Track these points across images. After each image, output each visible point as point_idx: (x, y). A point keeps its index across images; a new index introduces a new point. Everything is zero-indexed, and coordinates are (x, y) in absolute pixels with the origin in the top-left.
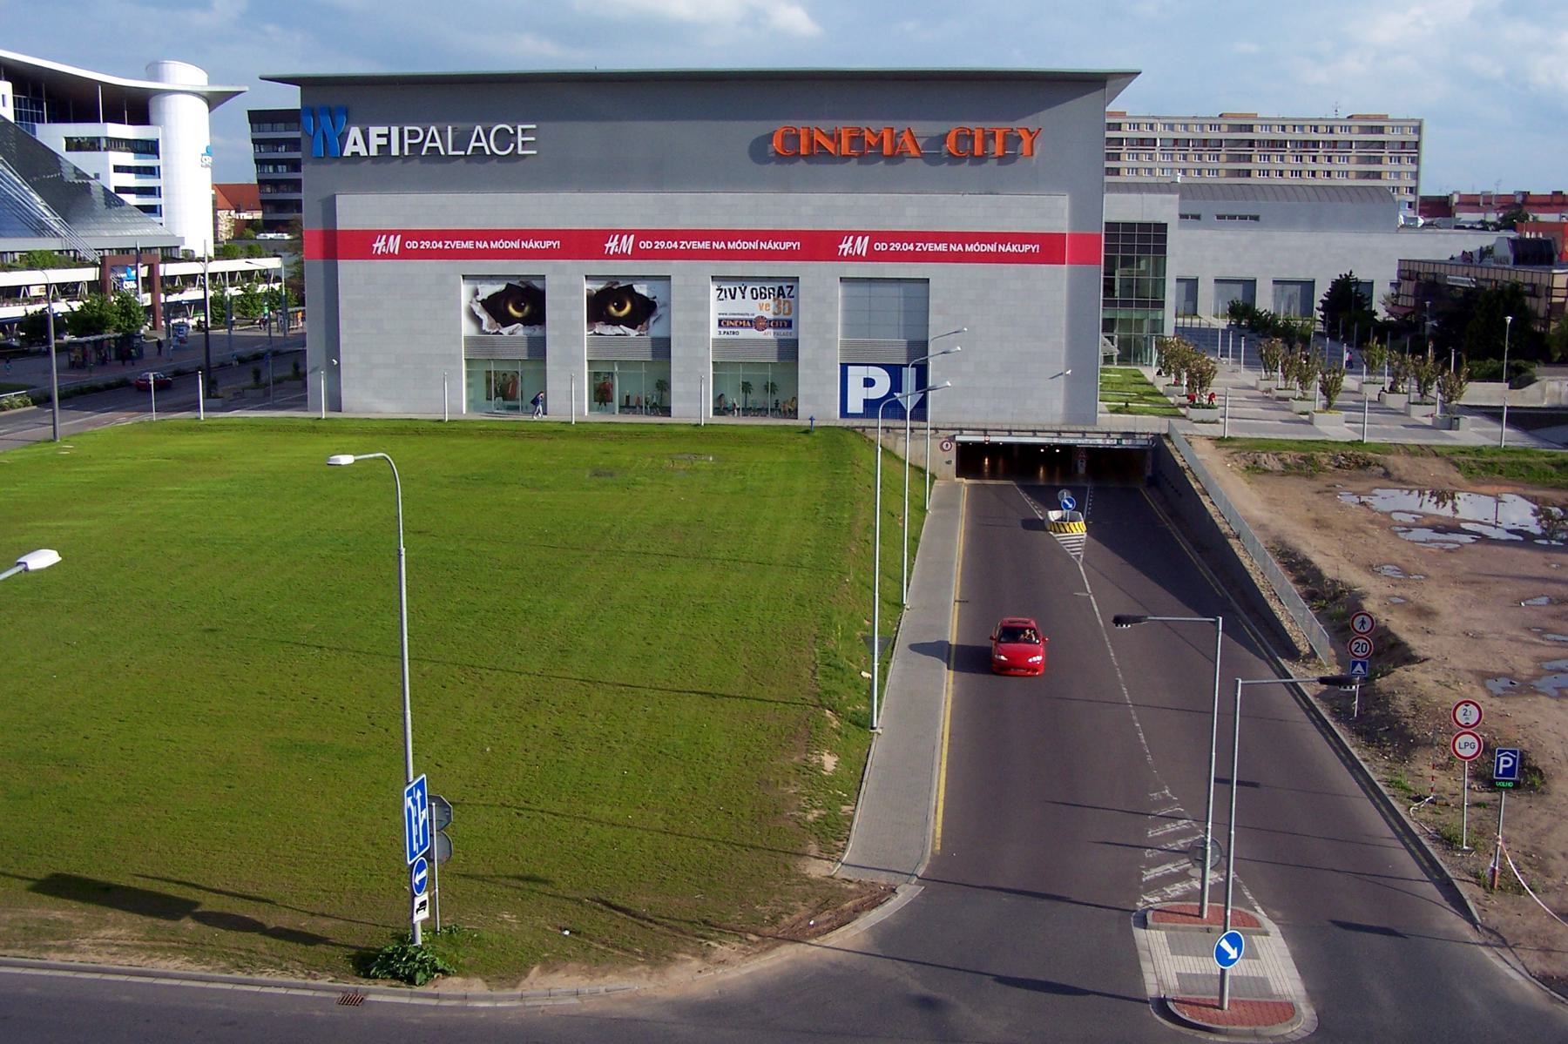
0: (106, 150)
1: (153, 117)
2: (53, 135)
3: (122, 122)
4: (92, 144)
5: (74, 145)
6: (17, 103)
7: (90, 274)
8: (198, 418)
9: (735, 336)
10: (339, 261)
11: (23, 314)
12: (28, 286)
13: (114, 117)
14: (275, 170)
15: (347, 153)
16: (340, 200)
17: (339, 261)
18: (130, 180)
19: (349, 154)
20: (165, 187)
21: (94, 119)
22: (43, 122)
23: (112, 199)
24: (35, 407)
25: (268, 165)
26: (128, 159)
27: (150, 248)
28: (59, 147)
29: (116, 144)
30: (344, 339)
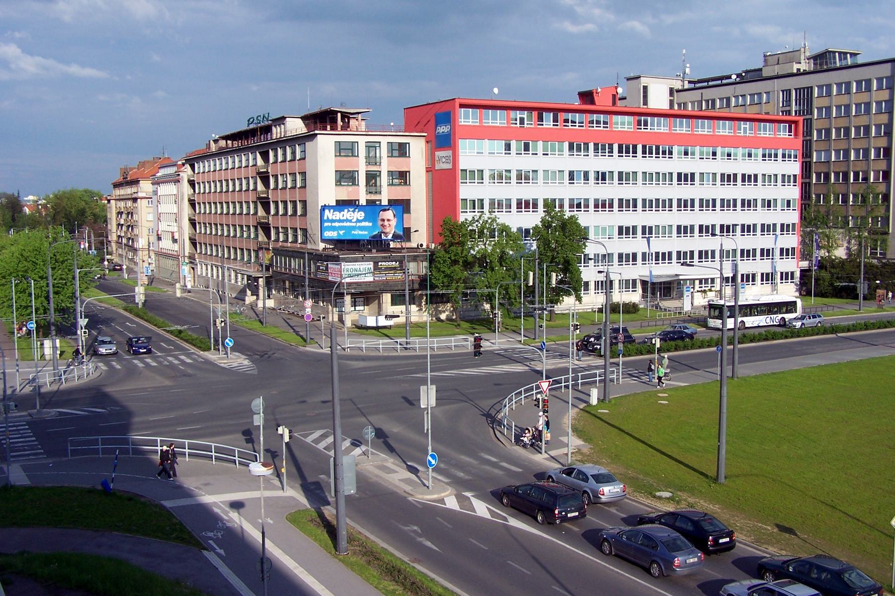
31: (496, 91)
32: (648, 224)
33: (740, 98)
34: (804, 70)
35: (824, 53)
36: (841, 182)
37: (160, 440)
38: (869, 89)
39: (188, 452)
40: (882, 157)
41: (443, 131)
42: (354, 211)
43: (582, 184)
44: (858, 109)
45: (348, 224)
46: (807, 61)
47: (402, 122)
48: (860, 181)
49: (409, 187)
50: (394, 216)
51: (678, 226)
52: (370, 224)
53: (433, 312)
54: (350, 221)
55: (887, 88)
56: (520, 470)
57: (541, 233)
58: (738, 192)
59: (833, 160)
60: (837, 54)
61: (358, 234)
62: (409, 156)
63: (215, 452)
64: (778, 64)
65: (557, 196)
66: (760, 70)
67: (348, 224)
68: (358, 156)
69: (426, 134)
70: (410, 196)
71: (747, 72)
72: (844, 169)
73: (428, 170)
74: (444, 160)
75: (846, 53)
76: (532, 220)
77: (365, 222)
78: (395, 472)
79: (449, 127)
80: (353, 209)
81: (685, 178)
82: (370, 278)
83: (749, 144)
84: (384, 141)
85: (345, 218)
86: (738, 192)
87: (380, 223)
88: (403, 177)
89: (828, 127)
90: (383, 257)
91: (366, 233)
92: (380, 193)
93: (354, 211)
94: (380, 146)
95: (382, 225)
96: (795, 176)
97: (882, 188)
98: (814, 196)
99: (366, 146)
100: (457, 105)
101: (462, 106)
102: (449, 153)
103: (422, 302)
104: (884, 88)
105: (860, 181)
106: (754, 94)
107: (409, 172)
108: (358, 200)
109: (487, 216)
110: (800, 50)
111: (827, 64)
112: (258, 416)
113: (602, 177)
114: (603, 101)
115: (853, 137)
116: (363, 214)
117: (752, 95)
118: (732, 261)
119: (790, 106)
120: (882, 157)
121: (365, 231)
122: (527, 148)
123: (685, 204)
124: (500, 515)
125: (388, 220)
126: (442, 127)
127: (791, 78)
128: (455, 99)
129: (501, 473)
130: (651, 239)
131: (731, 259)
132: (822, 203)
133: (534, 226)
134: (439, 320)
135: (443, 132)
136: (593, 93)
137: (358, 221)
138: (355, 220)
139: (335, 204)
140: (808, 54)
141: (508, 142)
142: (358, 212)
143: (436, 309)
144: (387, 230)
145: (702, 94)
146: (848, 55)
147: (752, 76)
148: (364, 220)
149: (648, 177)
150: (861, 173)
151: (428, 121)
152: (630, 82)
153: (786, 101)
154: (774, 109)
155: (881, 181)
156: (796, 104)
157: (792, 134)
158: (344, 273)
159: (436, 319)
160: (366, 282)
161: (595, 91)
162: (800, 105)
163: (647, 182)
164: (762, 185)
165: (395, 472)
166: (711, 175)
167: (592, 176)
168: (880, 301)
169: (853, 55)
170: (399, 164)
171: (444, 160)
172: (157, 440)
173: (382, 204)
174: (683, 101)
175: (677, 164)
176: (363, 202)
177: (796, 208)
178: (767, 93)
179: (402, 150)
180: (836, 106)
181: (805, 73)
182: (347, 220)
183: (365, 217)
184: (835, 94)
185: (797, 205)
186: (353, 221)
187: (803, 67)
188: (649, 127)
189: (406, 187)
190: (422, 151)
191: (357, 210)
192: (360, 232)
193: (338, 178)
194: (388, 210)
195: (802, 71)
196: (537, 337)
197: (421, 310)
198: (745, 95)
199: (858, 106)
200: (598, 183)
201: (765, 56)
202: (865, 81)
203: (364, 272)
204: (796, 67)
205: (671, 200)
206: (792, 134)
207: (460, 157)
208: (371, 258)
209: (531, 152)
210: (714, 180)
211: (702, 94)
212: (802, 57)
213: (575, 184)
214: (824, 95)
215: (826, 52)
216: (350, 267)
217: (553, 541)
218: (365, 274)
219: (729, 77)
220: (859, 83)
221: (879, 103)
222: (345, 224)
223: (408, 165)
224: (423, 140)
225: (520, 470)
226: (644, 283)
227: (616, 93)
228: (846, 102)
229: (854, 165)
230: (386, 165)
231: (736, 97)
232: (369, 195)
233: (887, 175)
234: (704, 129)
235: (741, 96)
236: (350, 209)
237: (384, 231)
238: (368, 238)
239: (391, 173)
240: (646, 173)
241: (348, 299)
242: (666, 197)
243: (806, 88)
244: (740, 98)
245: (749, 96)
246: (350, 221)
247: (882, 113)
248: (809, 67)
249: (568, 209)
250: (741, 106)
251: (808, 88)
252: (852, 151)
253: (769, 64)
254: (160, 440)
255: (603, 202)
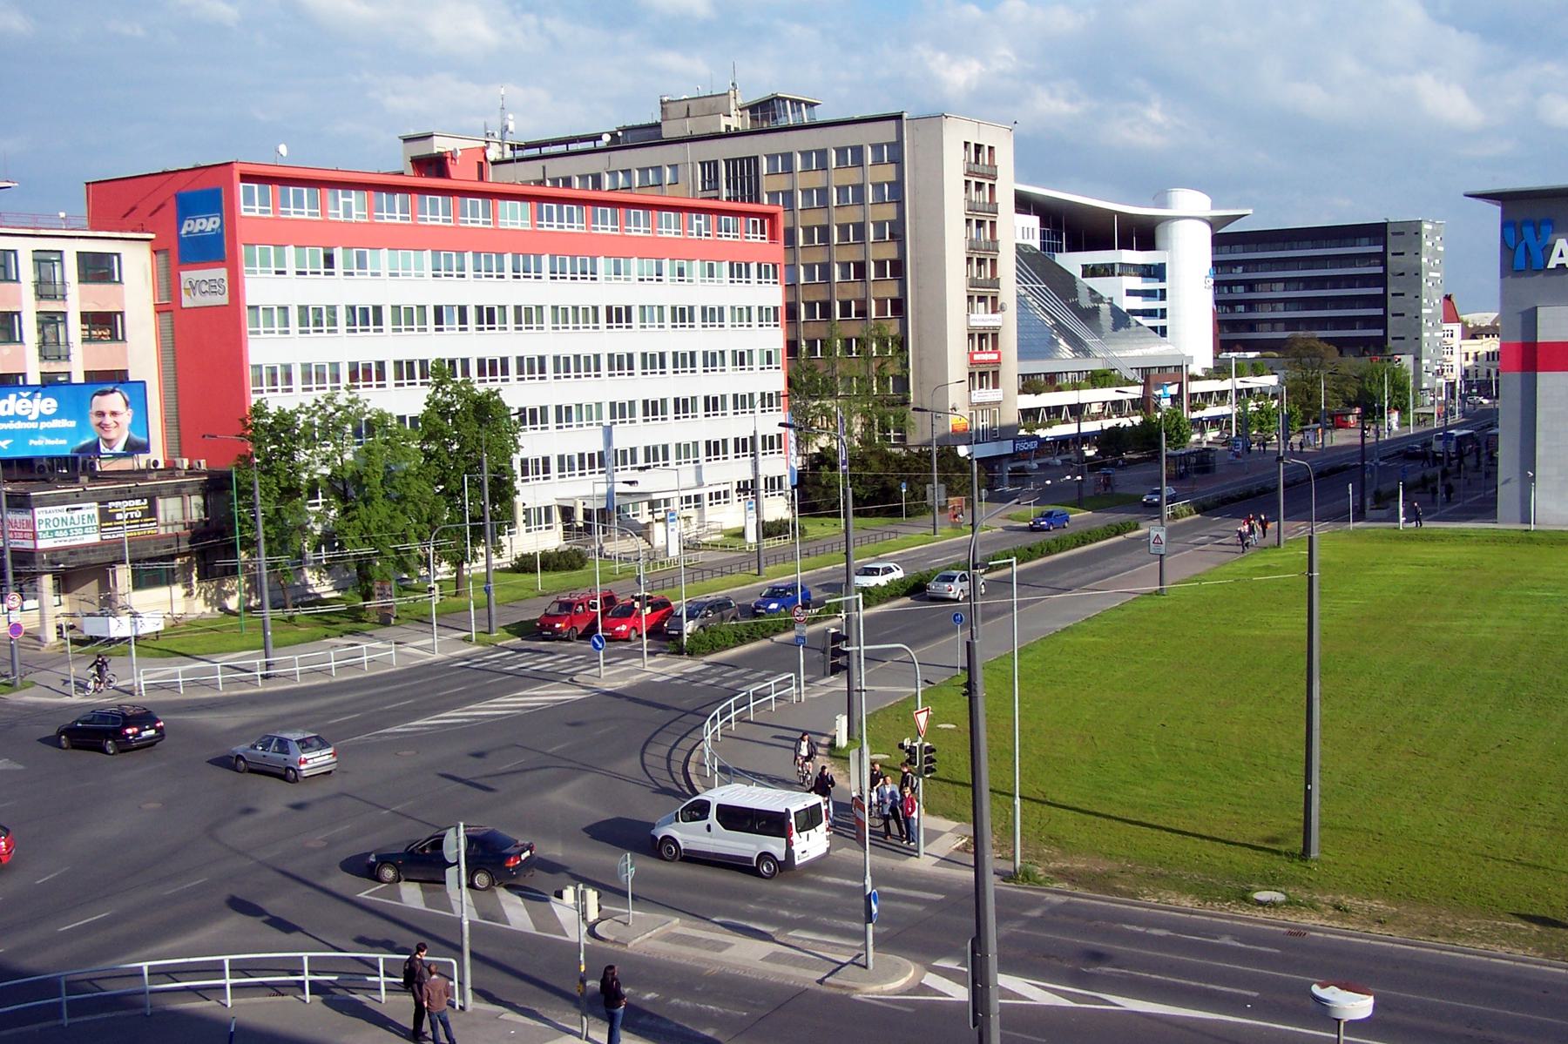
0: (1120, 275)
1: (1159, 242)
2: (1072, 262)
3: (1132, 249)
4: (1107, 270)
5: (1091, 271)
6: (1043, 235)
7: (1136, 392)
8: (1398, 528)
9: (38, 652)
10: (1538, 373)
11: (1100, 429)
12: (1090, 404)
13: (1126, 244)
14: (1230, 291)
15: (1551, 265)
16: (1541, 312)
17: (1538, 373)
18: (1138, 303)
19: (1554, 266)
20: (1170, 308)
21: (1108, 246)
22: (1061, 251)
23: (1121, 319)
24: (1198, 516)
25: (1224, 285)
26: (1137, 283)
27: (1166, 367)
28: (1077, 272)
29: (1127, 269)
30: (1540, 451)
31: (283, 149)
32: (565, 403)
33: (621, 175)
34: (736, 129)
35: (769, 101)
36: (818, 318)
37: (310, 958)
38: (823, 166)
39: (224, 978)
40: (888, 277)
41: (202, 228)
42: (31, 398)
43: (457, 331)
44: (841, 196)
45: (19, 425)
46: (740, 113)
47: (82, 210)
48: (853, 317)
49: (123, 344)
50: (127, 404)
51: (557, 407)
52: (73, 424)
53: (213, 596)
54: (24, 419)
55: (891, 162)
56: (942, 897)
57: (431, 425)
58: (697, 339)
59: (802, 281)
60: (788, 102)
61: (43, 446)
62: (120, 281)
63: (312, 972)
64: (688, 116)
65: (457, 354)
66: (658, 126)
67: (19, 425)
68: (17, 280)
69: (152, 236)
70: (126, 363)
71: (625, 130)
72: (824, 297)
73: (160, 309)
74: (205, 288)
75: (802, 102)
76: (410, 401)
77: (60, 419)
78: (728, 945)
79: (218, 220)
80: (28, 393)
81: (619, 316)
82: (94, 538)
83: (654, 251)
84: (71, 249)
85: (10, 412)
86: (697, 339)
87: (95, 420)
88: (103, 324)
89: (825, 223)
90: (117, 491)
91: (64, 442)
92: (68, 358)
93: (31, 398)
94: (61, 261)
95: (99, 425)
96: (776, 309)
97: (893, 328)
98: (804, 343)
99: (34, 260)
100: (237, 177)
101: (245, 178)
102: (221, 273)
103: (191, 578)
104: (886, 161)
105: (853, 317)
106: (647, 169)
107: (122, 313)
108: (24, 375)
109: (342, 398)
110: (727, 94)
111: (774, 118)
112: (455, 869)
113: (487, 316)
114: (462, 174)
115: (836, 242)
116: (54, 403)
117: (644, 171)
118: (694, 462)
119: (717, 189)
120: (888, 277)
121: (61, 438)
122: (361, 263)
123: (621, 363)
124: (1087, 996)
125: (114, 414)
126: (198, 221)
127: (716, 142)
128: (232, 163)
129: (920, 908)
130: (614, 426)
131: (691, 459)
132: (819, 356)
133: (387, 411)
134: (224, 609)
135: (201, 231)
136: (446, 158)
137: (43, 417)
138: (35, 416)
139: (83, 381)
140: (740, 101)
141: (328, 252)
142: (42, 398)
143: (218, 588)
144: (112, 435)
145: (544, 168)
146: (803, 105)
147: (646, 136)
148: (58, 415)
149: (563, 315)
150: (853, 303)
151: (133, 209)
152: (410, 144)
153: (710, 182)
154: (689, 189)
155: (889, 315)
156: (728, 187)
157: (766, 236)
158: (40, 528)
159: (220, 610)
160: (87, 546)
161: (449, 155)
162: (735, 188)
163: (403, 327)
164: (553, 328)
165: (728, 945)
166: (656, 309)
167: (471, 315)
168: (955, 516)
169: (810, 105)
170: (100, 298)
171: (205, 288)
172: (301, 958)
173: (74, 381)
174: (564, 175)
175: (604, 292)
176: (34, 379)
177: (780, 365)
178: (674, 167)
179: (97, 269)
180: (803, 191)
181: (739, 134)
182: (16, 417)
183: (59, 408)
184: (799, 169)
185: (781, 358)
186: (30, 418)
187: (735, 122)
188: (555, 223)
189: (114, 345)
190: (146, 271)
191: (39, 395)
192: (49, 442)
193: (40, 326)
194: (113, 391)
195: (732, 129)
196: (494, 628)
197: (189, 594)
198: (660, 167)
199: (842, 190)
200: (482, 329)
201: (662, 102)
202: (853, 148)
203: (81, 525)
204: (724, 121)
205: (504, 361)
206: (766, 236)
207: (247, 281)
208: (94, 495)
209: (369, 271)
210: (463, 320)
211: (544, 168)
212: (733, 106)
213: (445, 332)
214: (780, 171)
215: (772, 99)
216: (51, 516)
217: (1317, 1036)
218: (84, 528)
219: (599, 137)
220: (841, 152)
221: (878, 187)
222: (11, 426)
223: (121, 298)
224: (145, 249)
225: (942, 897)
226: (567, 513)
227: (482, 160)
228: (821, 184)
229: (843, 291)
230: (78, 299)
231: (613, 174)
232: (46, 363)
233: (899, 306)
234: (638, 227)
235: (622, 171)
236: (22, 394)
237: (105, 436)
238: (68, 453)
239: (86, 317)
240: (399, 307)
241: (47, 582)
242: (590, 352)
243: (747, 158)
244: (621, 175)
245: (637, 172)
246: (24, 419)
247: (885, 202)
248: (744, 123)
249: (477, 378)
250: (622, 189)
251: (749, 159)
252: (836, 266)
253: (670, 116)
254: (310, 958)
255: (365, 367)
